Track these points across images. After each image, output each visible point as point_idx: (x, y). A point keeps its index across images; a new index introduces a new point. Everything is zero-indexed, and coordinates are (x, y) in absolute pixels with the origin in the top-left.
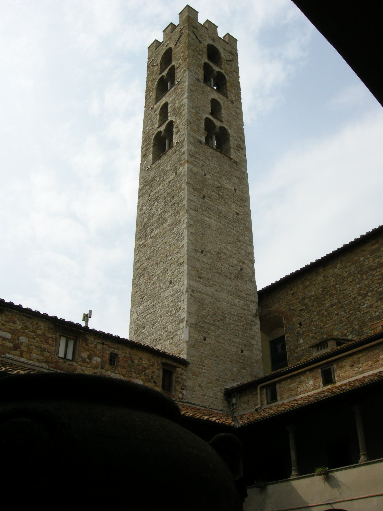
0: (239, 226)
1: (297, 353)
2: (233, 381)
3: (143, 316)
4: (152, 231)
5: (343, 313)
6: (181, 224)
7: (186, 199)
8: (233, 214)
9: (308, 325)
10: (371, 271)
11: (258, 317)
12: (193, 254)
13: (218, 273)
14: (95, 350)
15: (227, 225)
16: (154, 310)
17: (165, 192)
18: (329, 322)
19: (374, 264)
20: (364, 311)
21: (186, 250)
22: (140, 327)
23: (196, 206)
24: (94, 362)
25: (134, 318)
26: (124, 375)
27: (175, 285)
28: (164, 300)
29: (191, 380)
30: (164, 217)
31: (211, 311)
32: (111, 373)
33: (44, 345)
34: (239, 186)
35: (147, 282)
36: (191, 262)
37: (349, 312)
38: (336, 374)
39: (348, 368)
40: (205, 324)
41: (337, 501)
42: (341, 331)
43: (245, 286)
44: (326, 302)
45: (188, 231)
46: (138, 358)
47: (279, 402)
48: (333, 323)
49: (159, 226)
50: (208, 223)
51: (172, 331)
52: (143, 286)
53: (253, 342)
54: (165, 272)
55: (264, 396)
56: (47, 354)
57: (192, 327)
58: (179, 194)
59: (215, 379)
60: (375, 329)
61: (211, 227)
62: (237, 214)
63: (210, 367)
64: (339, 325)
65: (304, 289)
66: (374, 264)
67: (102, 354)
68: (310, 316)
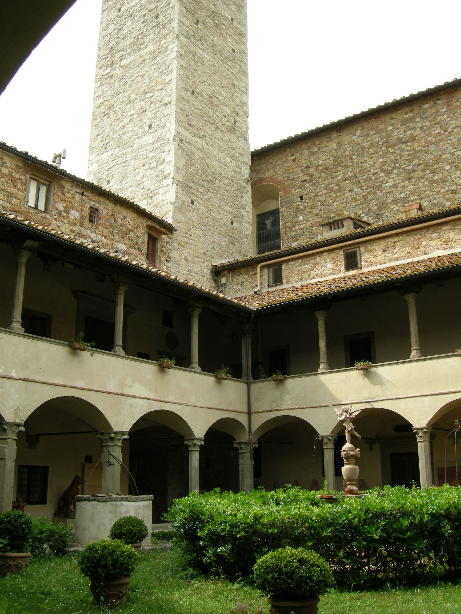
0: (234, 66)
1: (294, 232)
2: (221, 257)
3: (108, 167)
4: (122, 58)
5: (359, 189)
6: (168, 53)
7: (177, 21)
8: (229, 51)
9: (311, 200)
10: (400, 144)
11: (250, 183)
12: (183, 94)
13: (209, 122)
14: (72, 201)
15: (221, 63)
16: (124, 160)
17: (143, 9)
18: (340, 198)
19: (405, 137)
20: (385, 190)
21: (175, 87)
22: (102, 180)
23: (188, 32)
24: (72, 217)
25: (93, 169)
26: (105, 237)
27: (156, 131)
28: (139, 149)
29: (176, 251)
30: (141, 42)
31: (201, 168)
32: (91, 232)
33: (11, 189)
34: (236, 15)
35: (113, 124)
36: (180, 103)
37: (366, 189)
38: (362, 258)
39: (379, 252)
40: (193, 184)
41: (379, 399)
42: (354, 211)
43: (238, 143)
44: (337, 174)
45: (178, 63)
46: (121, 216)
47: (285, 286)
48: (345, 200)
49: (134, 53)
50: (201, 56)
51: (152, 188)
52: (108, 129)
53: (243, 213)
54: (142, 112)
55: (265, 277)
56: (15, 201)
57: (179, 186)
58: (167, 14)
59: (202, 252)
60: (408, 212)
61: (204, 62)
62: (234, 51)
63: (197, 238)
64: (353, 203)
65: (310, 156)
66: (405, 137)
67: (81, 207)
68: (315, 190)
